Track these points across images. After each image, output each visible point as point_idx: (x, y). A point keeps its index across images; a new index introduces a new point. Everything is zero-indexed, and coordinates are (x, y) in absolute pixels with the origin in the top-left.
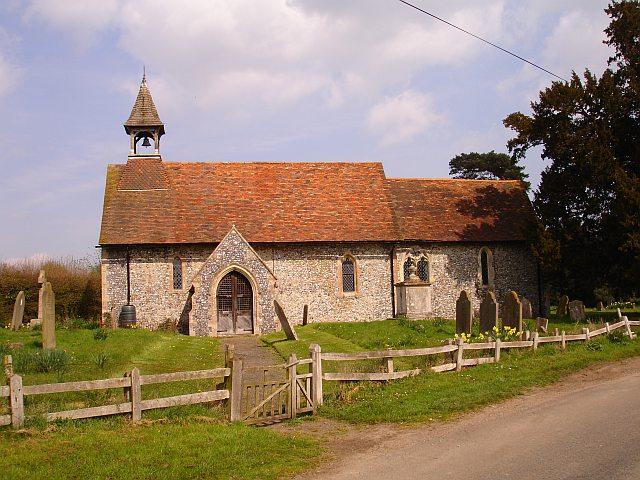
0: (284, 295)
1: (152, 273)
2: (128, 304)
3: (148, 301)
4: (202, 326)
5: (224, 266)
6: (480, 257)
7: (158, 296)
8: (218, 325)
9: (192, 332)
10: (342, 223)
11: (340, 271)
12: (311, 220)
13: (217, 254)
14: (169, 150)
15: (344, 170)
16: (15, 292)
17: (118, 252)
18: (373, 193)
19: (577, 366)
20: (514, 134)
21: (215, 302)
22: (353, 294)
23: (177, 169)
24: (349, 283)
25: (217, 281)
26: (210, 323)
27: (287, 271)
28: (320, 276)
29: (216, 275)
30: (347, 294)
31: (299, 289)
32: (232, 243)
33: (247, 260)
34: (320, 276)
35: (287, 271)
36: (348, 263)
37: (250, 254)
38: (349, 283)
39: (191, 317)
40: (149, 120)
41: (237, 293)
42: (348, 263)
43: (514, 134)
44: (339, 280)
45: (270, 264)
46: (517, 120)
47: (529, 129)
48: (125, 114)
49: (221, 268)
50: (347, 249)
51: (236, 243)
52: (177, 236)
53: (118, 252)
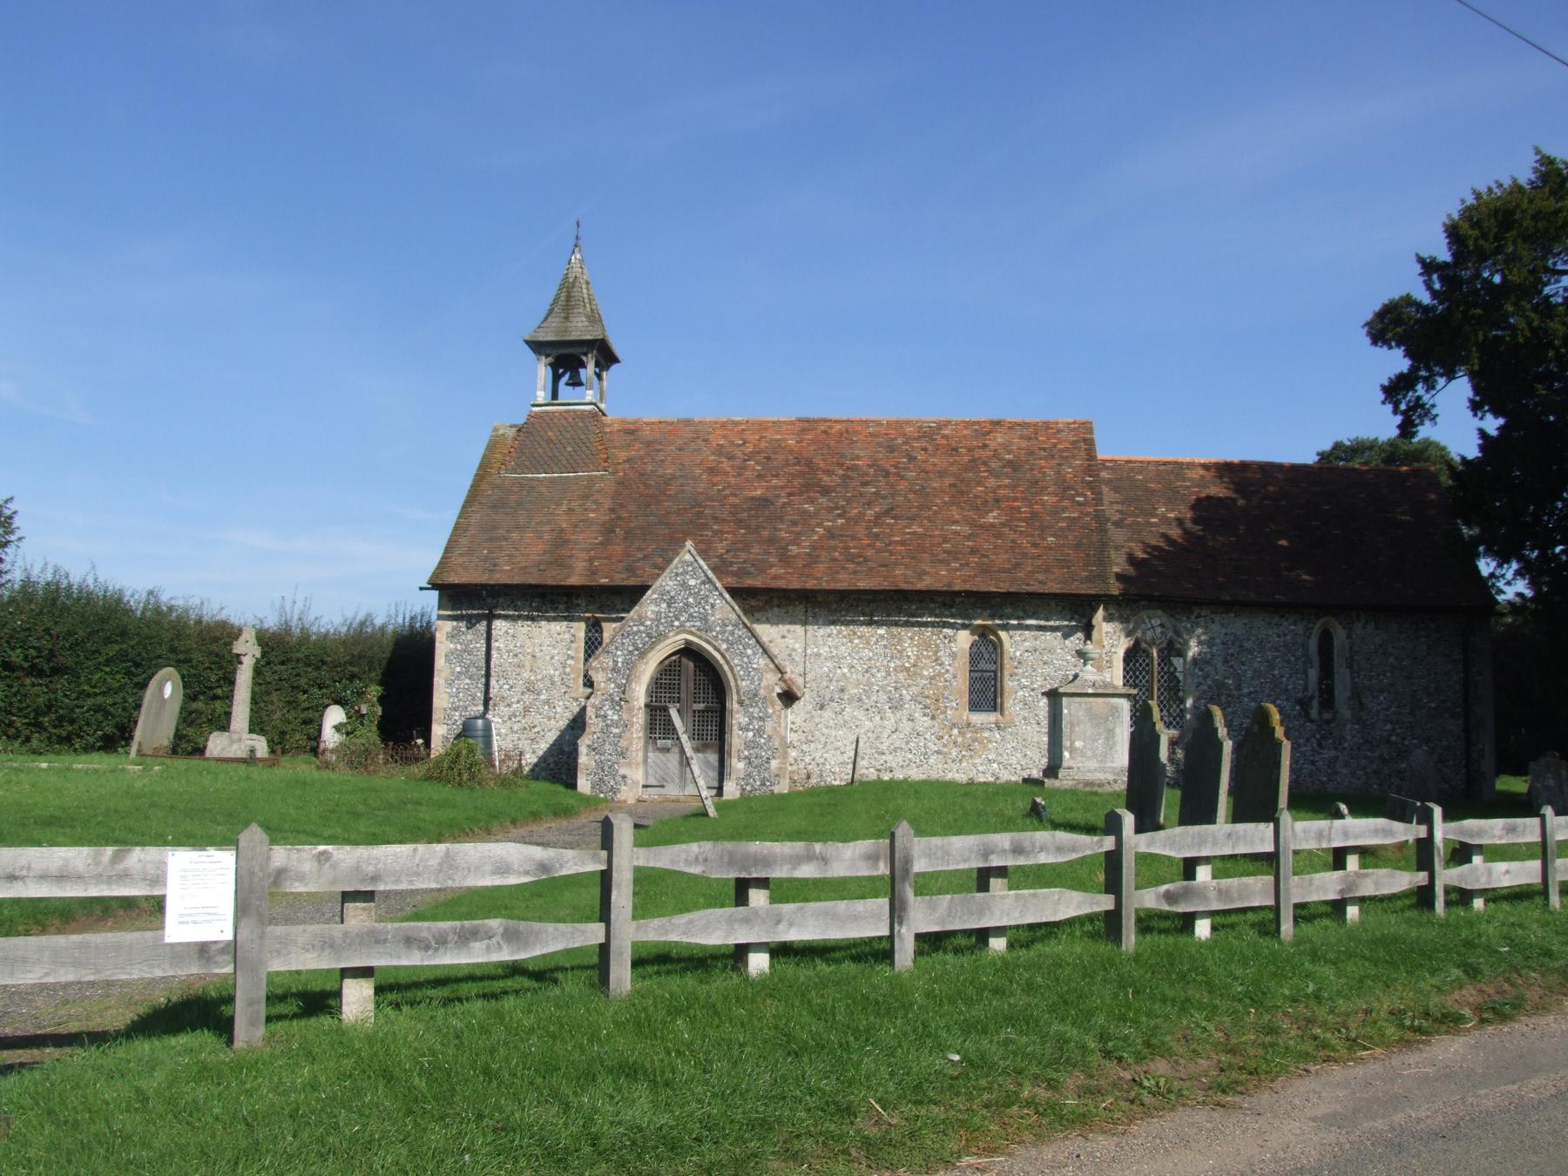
0: (828, 713)
1: (540, 649)
2: (483, 716)
3: (526, 710)
4: (604, 771)
5: (661, 637)
6: (1313, 644)
7: (547, 702)
8: (647, 773)
9: (584, 785)
10: (973, 551)
11: (963, 663)
12: (902, 543)
13: (649, 607)
14: (614, 397)
15: (1000, 438)
16: (139, 675)
17: (469, 598)
18: (1064, 488)
19: (418, 985)
20: (1396, 361)
21: (640, 719)
22: (992, 717)
23: (630, 432)
24: (986, 691)
25: (648, 669)
26: (633, 769)
27: (837, 660)
28: (912, 672)
29: (643, 654)
30: (978, 718)
31: (853, 703)
32: (684, 585)
33: (716, 621)
34: (912, 672)
35: (837, 660)
36: (595, 626)
37: (723, 609)
38: (986, 691)
39: (583, 750)
40: (579, 329)
41: (697, 692)
42: (595, 626)
43: (1396, 361)
44: (961, 683)
45: (766, 631)
46: (1398, 321)
47: (1424, 335)
48: (531, 313)
49: (656, 639)
50: (986, 606)
51: (692, 582)
52: (593, 572)
53: (469, 598)
